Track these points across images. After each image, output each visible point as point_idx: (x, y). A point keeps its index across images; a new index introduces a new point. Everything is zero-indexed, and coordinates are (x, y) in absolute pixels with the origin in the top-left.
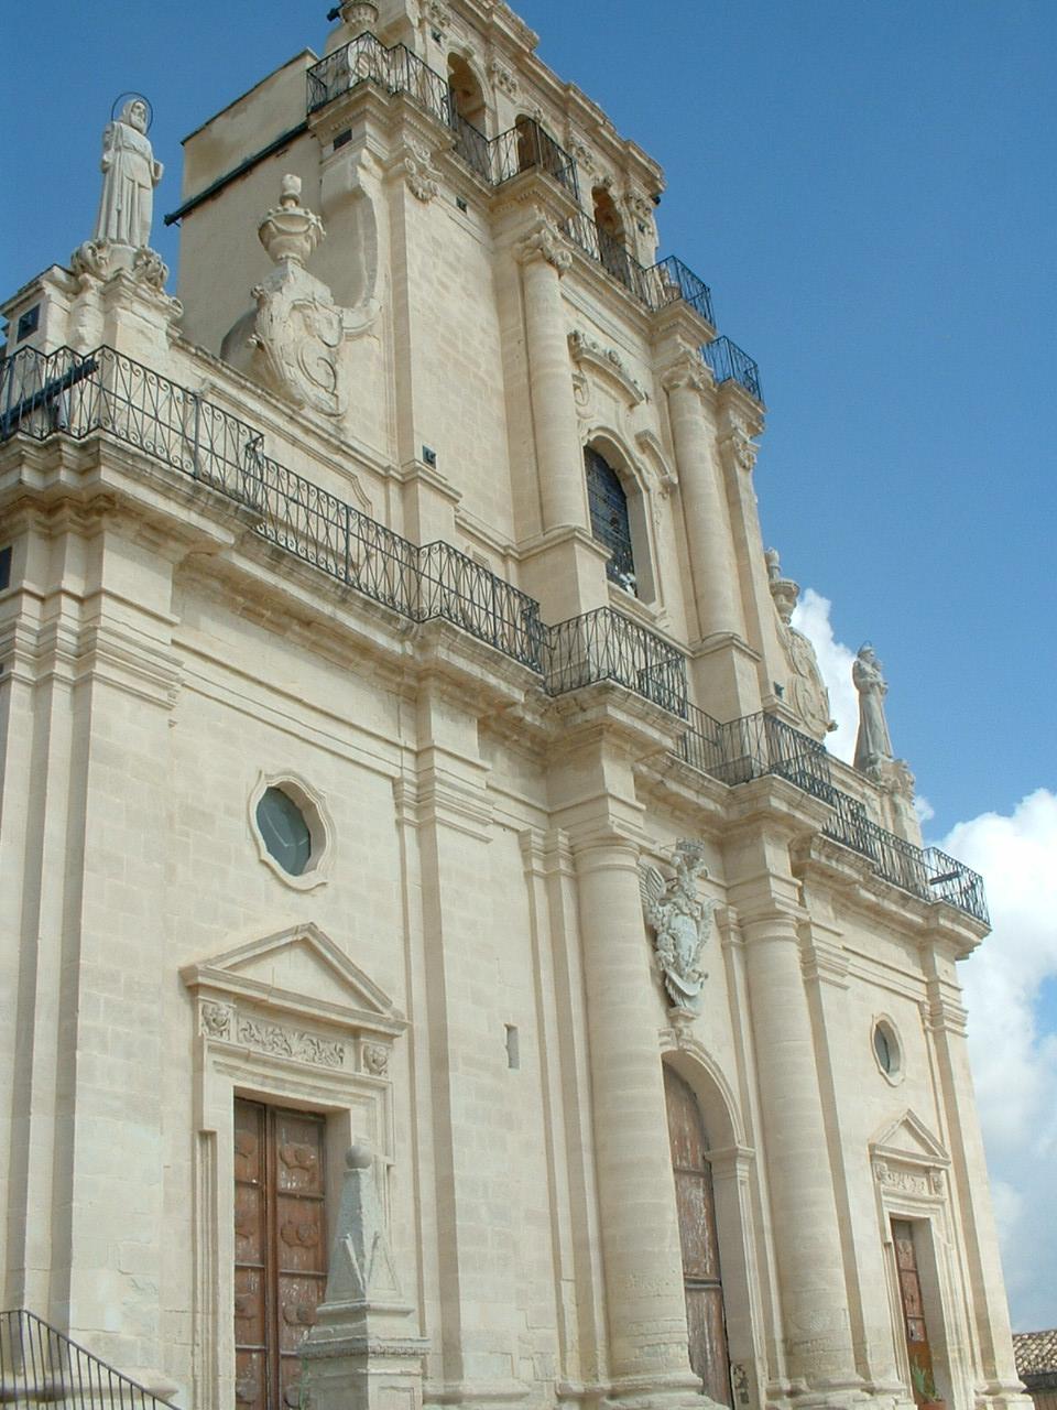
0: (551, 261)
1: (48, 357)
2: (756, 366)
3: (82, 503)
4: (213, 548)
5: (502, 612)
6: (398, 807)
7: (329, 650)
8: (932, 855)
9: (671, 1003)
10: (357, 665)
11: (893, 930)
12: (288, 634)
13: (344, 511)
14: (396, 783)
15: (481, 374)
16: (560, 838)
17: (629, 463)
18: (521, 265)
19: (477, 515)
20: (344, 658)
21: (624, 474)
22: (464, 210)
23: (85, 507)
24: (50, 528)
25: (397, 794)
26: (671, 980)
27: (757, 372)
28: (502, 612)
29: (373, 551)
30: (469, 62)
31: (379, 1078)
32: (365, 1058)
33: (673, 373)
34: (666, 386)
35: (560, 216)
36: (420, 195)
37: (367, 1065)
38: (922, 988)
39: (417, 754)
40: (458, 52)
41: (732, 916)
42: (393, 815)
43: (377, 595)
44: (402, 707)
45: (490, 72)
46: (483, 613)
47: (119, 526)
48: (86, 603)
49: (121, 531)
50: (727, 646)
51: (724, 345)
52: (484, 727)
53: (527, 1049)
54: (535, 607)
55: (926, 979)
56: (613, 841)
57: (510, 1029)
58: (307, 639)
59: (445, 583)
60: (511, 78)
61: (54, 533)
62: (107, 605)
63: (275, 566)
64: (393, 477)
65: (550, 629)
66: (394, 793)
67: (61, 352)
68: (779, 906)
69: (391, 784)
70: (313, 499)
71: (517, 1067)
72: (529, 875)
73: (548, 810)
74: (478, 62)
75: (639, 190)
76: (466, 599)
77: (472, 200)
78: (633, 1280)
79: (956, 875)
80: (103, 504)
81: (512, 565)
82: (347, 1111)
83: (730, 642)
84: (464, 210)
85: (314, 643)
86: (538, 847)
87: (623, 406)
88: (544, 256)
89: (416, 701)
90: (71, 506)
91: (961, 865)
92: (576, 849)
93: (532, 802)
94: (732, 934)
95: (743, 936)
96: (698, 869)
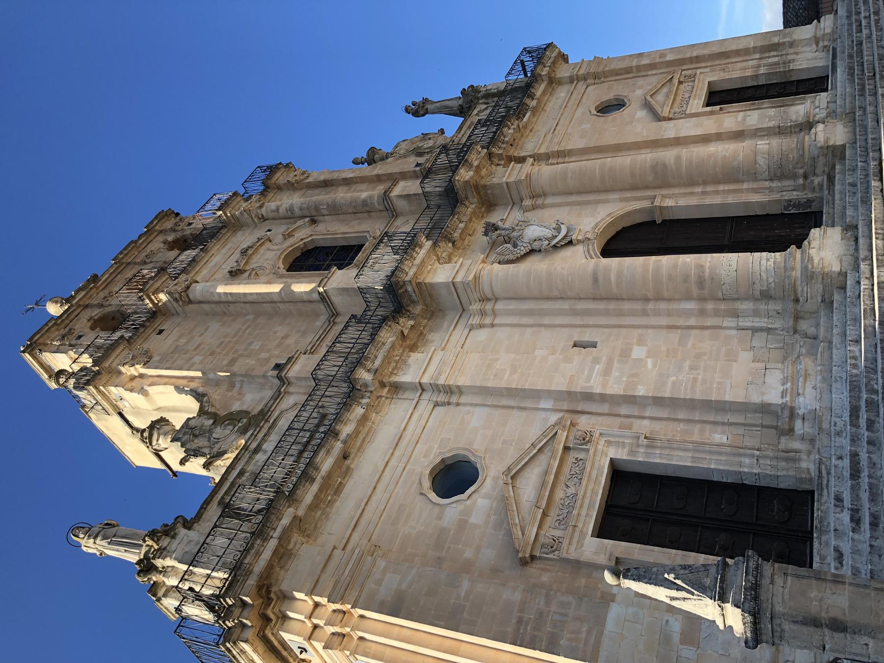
0: (188, 288)
1: (317, 385)
2: (259, 167)
3: (263, 603)
4: (296, 519)
5: (353, 338)
6: (449, 404)
7: (363, 441)
8: (509, 78)
9: (570, 243)
10: (373, 423)
11: (547, 100)
12: (352, 466)
13: (290, 431)
14: (437, 404)
15: (244, 328)
16: (527, 203)
17: (298, 245)
18: (190, 302)
19: (306, 342)
20: (368, 432)
21: (304, 247)
22: (163, 330)
23: (266, 600)
24: (278, 618)
25: (443, 404)
26: (557, 243)
27: (263, 167)
28: (353, 338)
29: (320, 404)
30: (96, 318)
31: (586, 447)
32: (582, 445)
33: (255, 217)
34: (262, 220)
35: (167, 279)
36: (148, 360)
37: (586, 444)
38: (581, 83)
39: (423, 390)
40: (89, 324)
41: (527, 202)
42: (452, 408)
43: (336, 414)
44: (399, 396)
45: (101, 306)
46: (363, 333)
47: (277, 580)
48: (465, 309)
49: (281, 578)
50: (389, 198)
51: (247, 185)
52: (413, 348)
53: (587, 336)
54: (354, 316)
55: (576, 82)
56: (477, 278)
57: (575, 345)
58: (356, 454)
59: (340, 363)
60: (106, 295)
61: (280, 615)
62: (425, 380)
63: (312, 478)
64: (285, 389)
65: (367, 305)
66: (442, 405)
67: (314, 376)
68: (471, 277)
69: (437, 407)
70: (311, 403)
71: (596, 343)
72: (492, 325)
73: (420, 391)
74: (96, 313)
75: (169, 224)
76: (361, 334)
77: (158, 326)
78: (684, 379)
79: (522, 62)
80: (264, 591)
81: (337, 320)
82: (611, 459)
83: (386, 195)
84: (163, 330)
85: (359, 450)
86: (479, 320)
87: (268, 245)
88: (185, 291)
89: (397, 388)
90: (265, 609)
91: (516, 61)
92: (481, 299)
93: (456, 321)
94: (537, 203)
95: (539, 196)
96: (500, 223)
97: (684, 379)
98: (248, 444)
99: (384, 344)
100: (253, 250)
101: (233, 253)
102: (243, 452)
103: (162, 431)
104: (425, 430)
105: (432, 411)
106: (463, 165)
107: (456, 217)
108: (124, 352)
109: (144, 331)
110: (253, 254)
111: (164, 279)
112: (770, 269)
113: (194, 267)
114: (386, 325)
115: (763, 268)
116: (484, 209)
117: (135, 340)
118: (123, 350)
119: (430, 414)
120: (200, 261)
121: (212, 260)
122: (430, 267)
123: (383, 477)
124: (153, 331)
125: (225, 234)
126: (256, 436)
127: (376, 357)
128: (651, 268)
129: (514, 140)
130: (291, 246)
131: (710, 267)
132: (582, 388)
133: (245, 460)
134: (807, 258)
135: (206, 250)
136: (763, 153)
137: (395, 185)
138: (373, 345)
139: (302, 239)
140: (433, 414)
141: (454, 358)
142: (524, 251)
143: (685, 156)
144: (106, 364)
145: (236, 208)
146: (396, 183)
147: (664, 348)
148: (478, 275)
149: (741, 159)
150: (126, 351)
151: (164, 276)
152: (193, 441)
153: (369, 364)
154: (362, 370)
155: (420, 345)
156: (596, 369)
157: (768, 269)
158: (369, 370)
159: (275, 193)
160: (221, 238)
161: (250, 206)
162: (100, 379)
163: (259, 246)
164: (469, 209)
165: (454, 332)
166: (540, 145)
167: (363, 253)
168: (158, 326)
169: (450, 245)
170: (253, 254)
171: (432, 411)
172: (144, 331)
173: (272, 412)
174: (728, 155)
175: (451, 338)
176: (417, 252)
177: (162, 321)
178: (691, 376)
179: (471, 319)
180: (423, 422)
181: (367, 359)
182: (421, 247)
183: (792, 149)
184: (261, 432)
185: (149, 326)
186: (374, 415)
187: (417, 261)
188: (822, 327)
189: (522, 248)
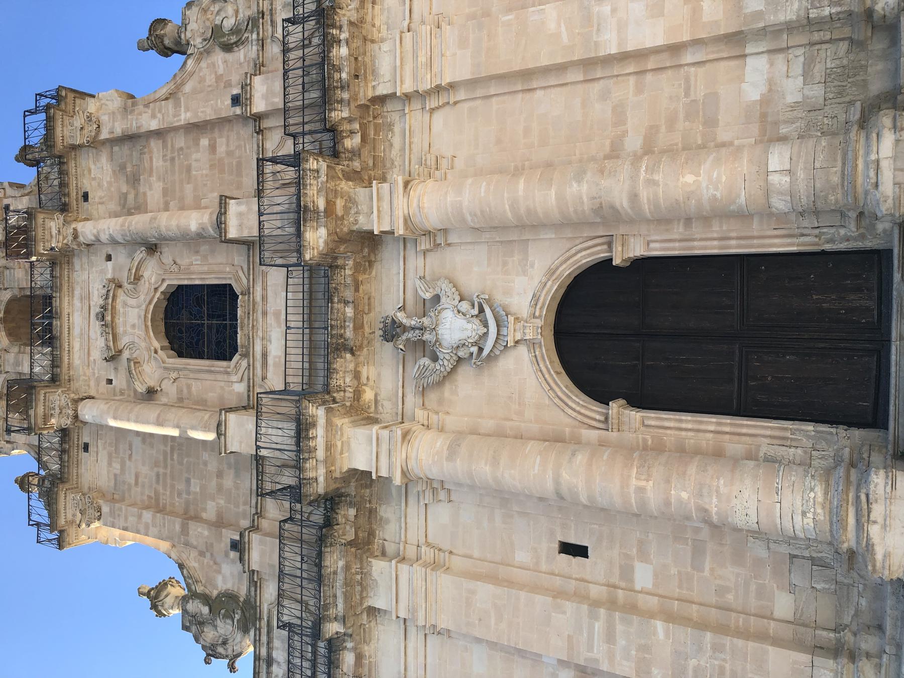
20: (370, 671)
77: (78, 441)
97: (708, 665)
98: (258, 653)
99: (335, 573)
100: (110, 312)
101: (90, 307)
102: (257, 663)
103: (166, 606)
104: (427, 666)
105: (425, 641)
106: (305, 221)
107: (336, 300)
108: (68, 498)
109: (69, 457)
110: (113, 318)
111: (42, 398)
112: (809, 529)
113: (60, 346)
114: (326, 547)
115: (797, 527)
116: (366, 250)
117: (68, 473)
118: (65, 496)
119: (425, 646)
120: (61, 333)
121: (73, 324)
122: (339, 444)
123: (408, 665)
124: (62, 127)
125: (61, 275)
126: (260, 640)
127: (335, 596)
128: (633, 501)
129: (356, 59)
130: (150, 303)
131: (717, 513)
132: (586, 660)
133: (265, 671)
134: (865, 539)
135: (57, 313)
136: (781, 193)
137: (225, 213)
138: (324, 585)
139: (156, 289)
140: (428, 645)
141: (424, 583)
142: (450, 365)
143: (645, 194)
144: (62, 521)
145: (46, 238)
146: (225, 208)
147: (674, 571)
148: (405, 469)
149: (744, 203)
150: (71, 496)
151: (39, 393)
152: (203, 632)
153: (332, 612)
154: (328, 624)
155: (375, 527)
156: (596, 629)
157: (805, 528)
158: (335, 618)
159: (75, 159)
160: (61, 284)
161: (61, 238)
162: (68, 535)
163: (112, 302)
164: (348, 394)
165: (408, 509)
166: (401, 68)
167: (242, 329)
168: (78, 441)
169: (348, 356)
170: (113, 318)
171: (425, 641)
172: (69, 457)
173: (253, 293)
174: (718, 195)
175: (408, 520)
176: (313, 438)
177: (78, 433)
178: (716, 662)
179: (421, 498)
180: (421, 659)
181: (326, 607)
182: (314, 425)
183: (834, 189)
184: (262, 634)
185: (70, 447)
186: (366, 648)
187: (320, 454)
188: (888, 618)
189: (446, 363)
